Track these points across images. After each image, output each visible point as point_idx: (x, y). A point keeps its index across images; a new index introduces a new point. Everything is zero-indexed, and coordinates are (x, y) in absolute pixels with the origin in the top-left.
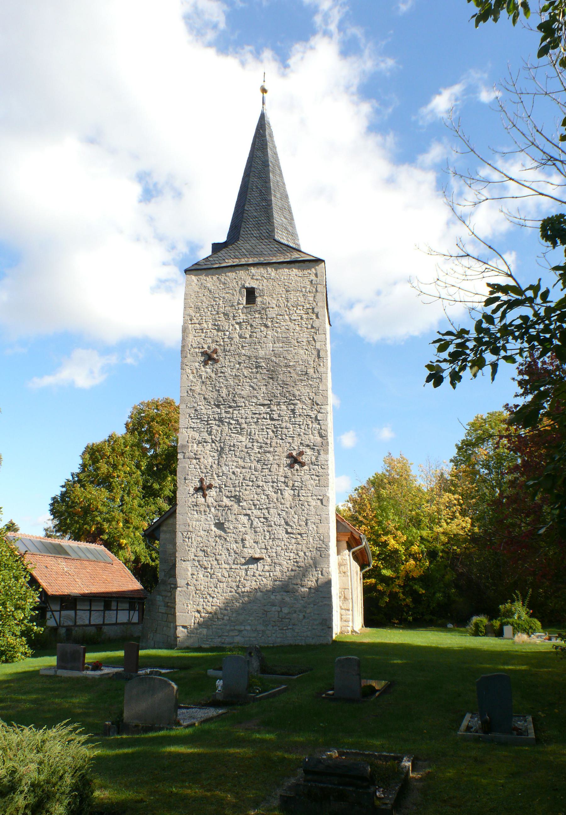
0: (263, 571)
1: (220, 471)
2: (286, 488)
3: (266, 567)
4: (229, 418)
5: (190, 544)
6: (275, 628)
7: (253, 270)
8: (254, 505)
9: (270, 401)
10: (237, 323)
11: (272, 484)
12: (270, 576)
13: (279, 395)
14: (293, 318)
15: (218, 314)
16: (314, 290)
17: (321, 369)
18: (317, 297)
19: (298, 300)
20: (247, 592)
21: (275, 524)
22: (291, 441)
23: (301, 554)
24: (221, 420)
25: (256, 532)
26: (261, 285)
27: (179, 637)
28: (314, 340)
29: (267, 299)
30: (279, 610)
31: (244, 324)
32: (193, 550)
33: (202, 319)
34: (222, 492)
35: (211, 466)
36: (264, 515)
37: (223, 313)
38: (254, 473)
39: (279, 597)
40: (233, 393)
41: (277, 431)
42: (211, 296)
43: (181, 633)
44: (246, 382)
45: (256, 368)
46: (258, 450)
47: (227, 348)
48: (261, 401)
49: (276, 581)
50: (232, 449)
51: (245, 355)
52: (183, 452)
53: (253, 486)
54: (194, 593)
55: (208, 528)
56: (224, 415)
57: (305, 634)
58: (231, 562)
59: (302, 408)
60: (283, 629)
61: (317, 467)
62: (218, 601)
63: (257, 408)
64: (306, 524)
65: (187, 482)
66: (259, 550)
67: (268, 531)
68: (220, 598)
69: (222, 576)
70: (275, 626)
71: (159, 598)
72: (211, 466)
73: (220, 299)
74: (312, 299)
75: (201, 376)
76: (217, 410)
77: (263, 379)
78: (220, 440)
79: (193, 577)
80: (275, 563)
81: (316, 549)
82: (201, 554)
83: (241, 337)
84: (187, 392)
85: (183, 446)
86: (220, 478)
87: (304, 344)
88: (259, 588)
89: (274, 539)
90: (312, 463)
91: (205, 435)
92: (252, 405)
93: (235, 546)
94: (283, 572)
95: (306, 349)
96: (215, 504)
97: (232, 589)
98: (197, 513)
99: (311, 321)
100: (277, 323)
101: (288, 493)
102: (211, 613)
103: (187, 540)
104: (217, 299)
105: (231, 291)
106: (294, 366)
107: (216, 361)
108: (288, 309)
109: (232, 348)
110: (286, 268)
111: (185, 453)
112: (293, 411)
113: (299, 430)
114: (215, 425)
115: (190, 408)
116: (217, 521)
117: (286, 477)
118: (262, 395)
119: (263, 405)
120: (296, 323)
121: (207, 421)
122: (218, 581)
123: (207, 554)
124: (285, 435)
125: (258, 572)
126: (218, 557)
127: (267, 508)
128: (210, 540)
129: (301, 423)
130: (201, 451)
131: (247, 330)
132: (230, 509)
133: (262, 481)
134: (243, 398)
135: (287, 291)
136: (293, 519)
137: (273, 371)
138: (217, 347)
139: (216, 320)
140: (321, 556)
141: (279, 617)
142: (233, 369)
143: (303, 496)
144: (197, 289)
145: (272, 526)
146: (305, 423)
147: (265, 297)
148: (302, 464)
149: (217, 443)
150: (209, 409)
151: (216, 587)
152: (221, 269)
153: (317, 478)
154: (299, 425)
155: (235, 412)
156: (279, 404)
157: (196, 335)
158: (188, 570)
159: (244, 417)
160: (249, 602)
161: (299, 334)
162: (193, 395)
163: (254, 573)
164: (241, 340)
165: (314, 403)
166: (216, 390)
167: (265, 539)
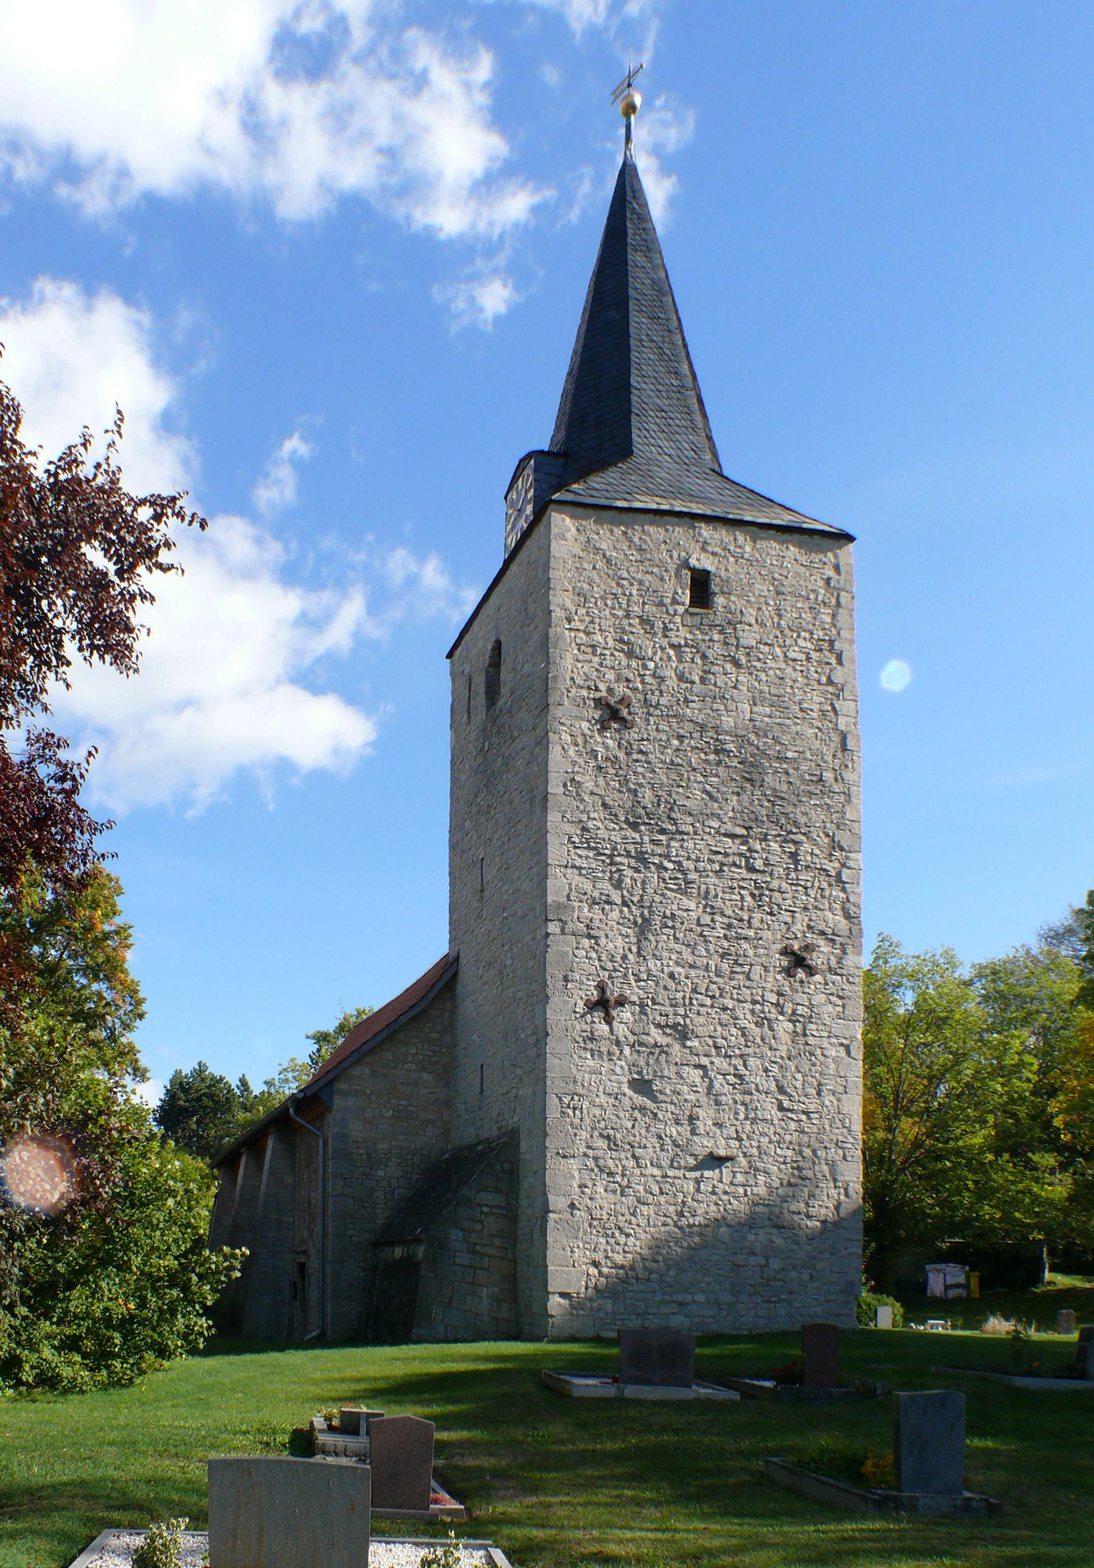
0: (732, 1183)
1: (643, 969)
2: (781, 1018)
3: (738, 1175)
4: (660, 855)
5: (577, 1121)
6: (754, 1298)
7: (706, 531)
8: (716, 1047)
9: (748, 828)
10: (672, 646)
11: (751, 1007)
12: (746, 1195)
13: (765, 819)
14: (791, 655)
15: (628, 616)
16: (834, 601)
17: (848, 776)
18: (839, 618)
19: (800, 617)
20: (700, 1225)
21: (758, 1091)
22: (789, 920)
23: (807, 1152)
24: (641, 858)
25: (718, 1103)
26: (723, 569)
27: (552, 1316)
28: (834, 709)
29: (735, 602)
30: (763, 1262)
31: (688, 650)
32: (584, 1135)
33: (592, 622)
34: (646, 1014)
35: (624, 957)
36: (736, 1069)
37: (640, 617)
38: (715, 979)
39: (763, 1237)
40: (666, 802)
41: (761, 895)
42: (610, 572)
43: (556, 1304)
44: (696, 781)
45: (717, 752)
46: (722, 931)
47: (654, 699)
48: (729, 827)
49: (758, 1204)
50: (670, 924)
51: (691, 721)
52: (560, 920)
53: (712, 1006)
54: (586, 1225)
55: (616, 1090)
56: (648, 847)
57: (812, 1310)
58: (665, 1163)
59: (812, 854)
60: (770, 1302)
61: (839, 978)
62: (638, 1243)
63: (720, 841)
64: (819, 1093)
65: (569, 986)
66: (723, 1142)
67: (743, 1104)
68: (643, 1236)
69: (646, 1191)
70: (755, 1294)
71: (455, 1234)
72: (624, 957)
73: (632, 585)
74: (828, 619)
75: (593, 754)
76: (630, 833)
77: (733, 780)
78: (641, 900)
79: (583, 1192)
80: (757, 1170)
81: (837, 1144)
82: (601, 1143)
83: (681, 678)
84: (565, 785)
85: (559, 906)
86: (642, 983)
87: (814, 715)
88: (724, 1218)
89: (754, 1121)
90: (830, 970)
91: (606, 886)
92: (710, 833)
93: (673, 1130)
94: (771, 1187)
95: (818, 728)
96: (631, 1038)
97: (669, 1220)
98: (592, 1055)
99: (827, 668)
100: (759, 660)
101: (784, 1026)
102: (622, 1267)
103: (570, 1112)
104: (625, 583)
105: (655, 570)
106: (795, 760)
107: (626, 724)
108: (782, 632)
109: (664, 701)
110: (775, 541)
111: (564, 923)
112: (794, 856)
113: (804, 898)
114: (629, 866)
115: (572, 822)
116: (636, 1076)
117: (780, 994)
118: (731, 814)
119: (733, 836)
120: (798, 668)
121: (611, 856)
122: (639, 1201)
123: (615, 1145)
124: (778, 905)
125: (721, 1185)
126: (639, 1152)
127: (741, 1056)
128: (621, 1115)
129: (809, 884)
130: (601, 920)
131: (694, 666)
132: (666, 1053)
133: (732, 998)
134: (690, 814)
135: (778, 593)
136: (794, 1082)
137: (752, 765)
138: (628, 692)
139: (624, 631)
140: (844, 1158)
141: (762, 1278)
142: (665, 747)
143: (813, 1035)
144: (577, 550)
145: (751, 1094)
146: (816, 884)
147: (733, 598)
148: (811, 971)
149: (634, 908)
150: (614, 830)
151: (633, 1214)
152: (631, 515)
153: (840, 1002)
154: (806, 888)
155: (673, 843)
156: (764, 838)
157: (581, 657)
158: (573, 1177)
159: (693, 857)
160: (703, 1246)
161: (805, 692)
162: (578, 795)
163: (714, 1186)
164: (684, 686)
165: (836, 845)
166: (629, 790)
167: (737, 1119)
